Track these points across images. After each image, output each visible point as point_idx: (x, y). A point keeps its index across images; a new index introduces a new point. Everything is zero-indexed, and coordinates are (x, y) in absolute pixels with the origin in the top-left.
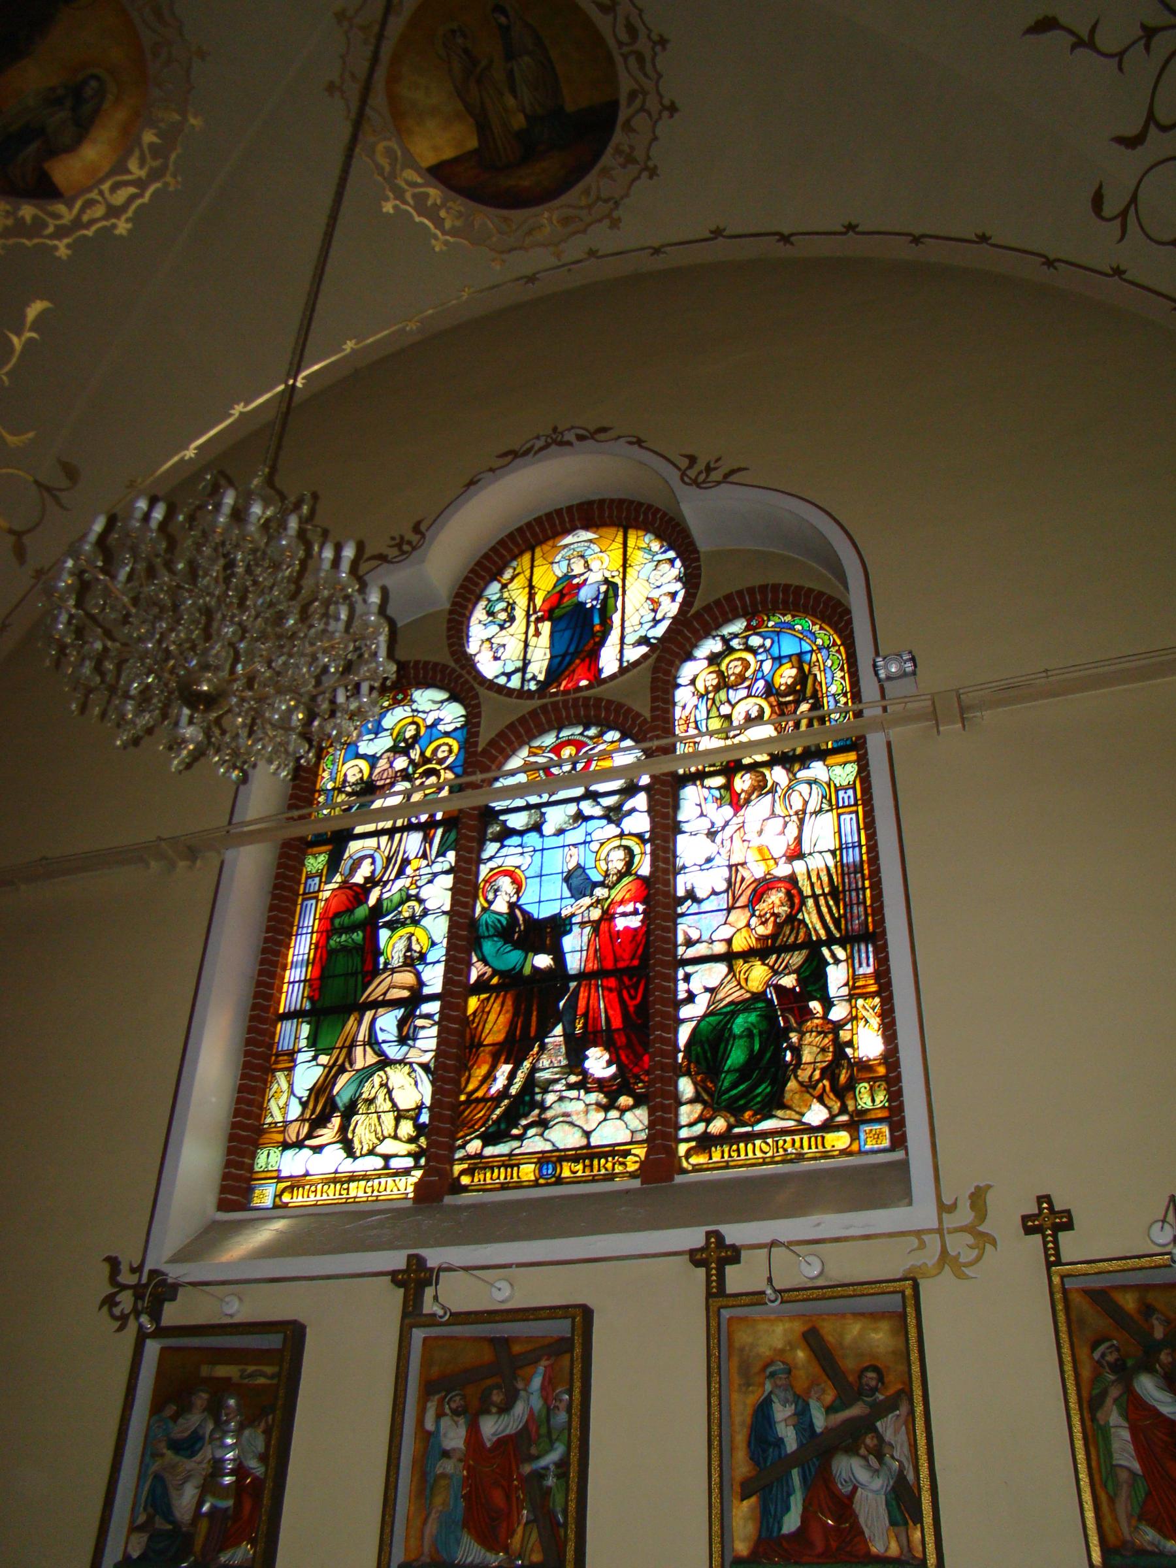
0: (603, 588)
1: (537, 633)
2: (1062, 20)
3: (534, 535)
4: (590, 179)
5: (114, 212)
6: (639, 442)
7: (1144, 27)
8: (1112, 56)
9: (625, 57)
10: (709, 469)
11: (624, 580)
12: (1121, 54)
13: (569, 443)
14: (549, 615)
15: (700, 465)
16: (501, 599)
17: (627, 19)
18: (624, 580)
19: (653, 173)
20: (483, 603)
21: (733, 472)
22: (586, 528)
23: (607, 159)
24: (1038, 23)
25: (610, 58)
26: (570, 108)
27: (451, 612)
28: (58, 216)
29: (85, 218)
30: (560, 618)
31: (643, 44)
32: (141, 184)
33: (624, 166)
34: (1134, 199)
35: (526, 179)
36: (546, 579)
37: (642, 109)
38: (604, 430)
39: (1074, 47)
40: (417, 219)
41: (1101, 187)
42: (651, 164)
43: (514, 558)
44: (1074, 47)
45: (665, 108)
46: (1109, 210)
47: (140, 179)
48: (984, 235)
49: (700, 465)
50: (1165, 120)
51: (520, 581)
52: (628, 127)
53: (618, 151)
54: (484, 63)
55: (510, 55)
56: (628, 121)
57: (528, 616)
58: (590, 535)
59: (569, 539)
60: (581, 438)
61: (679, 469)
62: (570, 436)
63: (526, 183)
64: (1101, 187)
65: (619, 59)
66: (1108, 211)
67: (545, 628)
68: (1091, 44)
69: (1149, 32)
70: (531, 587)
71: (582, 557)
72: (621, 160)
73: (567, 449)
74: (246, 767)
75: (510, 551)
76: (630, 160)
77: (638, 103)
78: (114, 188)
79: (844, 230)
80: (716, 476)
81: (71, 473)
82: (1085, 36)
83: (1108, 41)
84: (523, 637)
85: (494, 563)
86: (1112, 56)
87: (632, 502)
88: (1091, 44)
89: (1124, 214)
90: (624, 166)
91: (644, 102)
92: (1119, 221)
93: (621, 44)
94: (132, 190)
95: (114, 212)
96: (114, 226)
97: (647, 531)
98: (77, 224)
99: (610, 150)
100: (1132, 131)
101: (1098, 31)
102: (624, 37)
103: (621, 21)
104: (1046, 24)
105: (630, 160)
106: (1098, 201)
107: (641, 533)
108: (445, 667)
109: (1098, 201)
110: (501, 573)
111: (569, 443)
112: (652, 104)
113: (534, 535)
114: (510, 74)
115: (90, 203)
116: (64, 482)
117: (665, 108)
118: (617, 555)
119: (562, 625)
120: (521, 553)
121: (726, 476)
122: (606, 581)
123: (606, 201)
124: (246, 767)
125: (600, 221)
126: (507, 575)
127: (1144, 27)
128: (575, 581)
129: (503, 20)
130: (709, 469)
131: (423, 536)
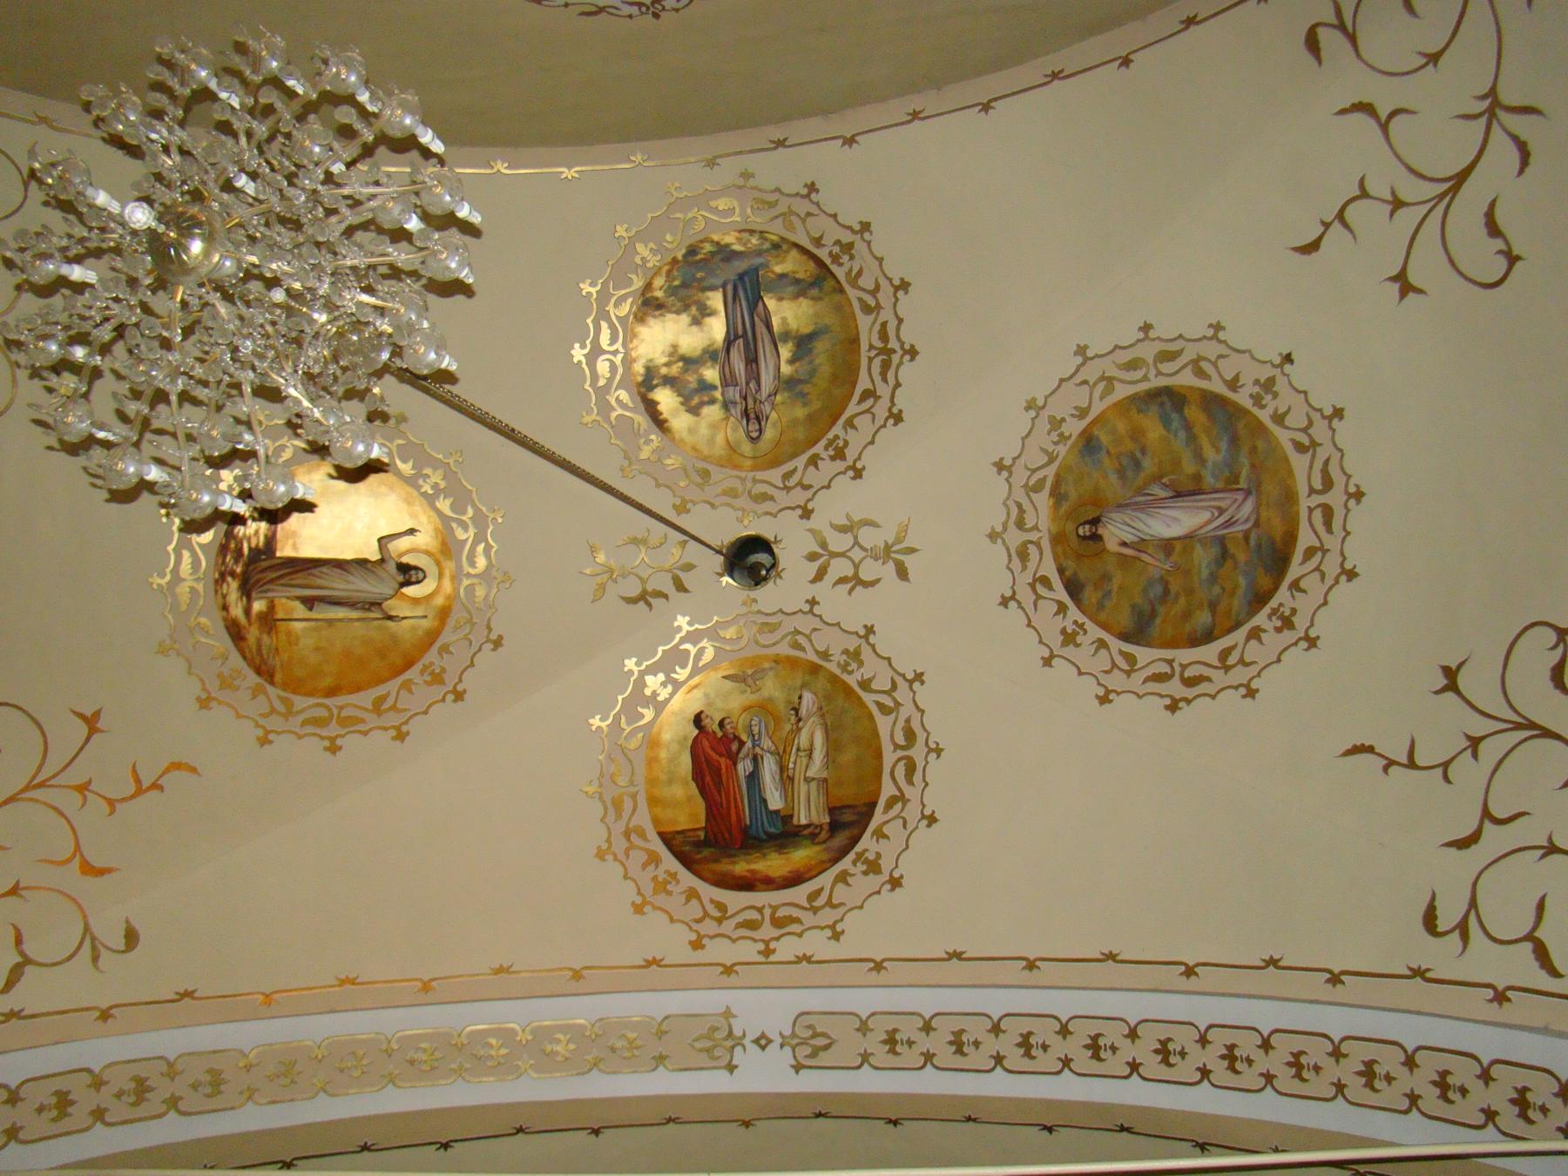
5: (596, 351)
12: (1446, 765)
29: (604, 325)
32: (602, 392)
34: (1473, 904)
39: (1386, 769)
40: (620, 698)
46: (1445, 921)
47: (608, 392)
48: (1500, 1004)
69: (1474, 743)
74: (281, 139)
77: (281, 708)
81: (1312, 44)
90: (852, 258)
91: (279, 713)
94: (602, 383)
95: (596, 351)
96: (583, 346)
98: (603, 315)
106: (1430, 920)
109: (1430, 920)
116: (1323, 34)
124: (281, 139)
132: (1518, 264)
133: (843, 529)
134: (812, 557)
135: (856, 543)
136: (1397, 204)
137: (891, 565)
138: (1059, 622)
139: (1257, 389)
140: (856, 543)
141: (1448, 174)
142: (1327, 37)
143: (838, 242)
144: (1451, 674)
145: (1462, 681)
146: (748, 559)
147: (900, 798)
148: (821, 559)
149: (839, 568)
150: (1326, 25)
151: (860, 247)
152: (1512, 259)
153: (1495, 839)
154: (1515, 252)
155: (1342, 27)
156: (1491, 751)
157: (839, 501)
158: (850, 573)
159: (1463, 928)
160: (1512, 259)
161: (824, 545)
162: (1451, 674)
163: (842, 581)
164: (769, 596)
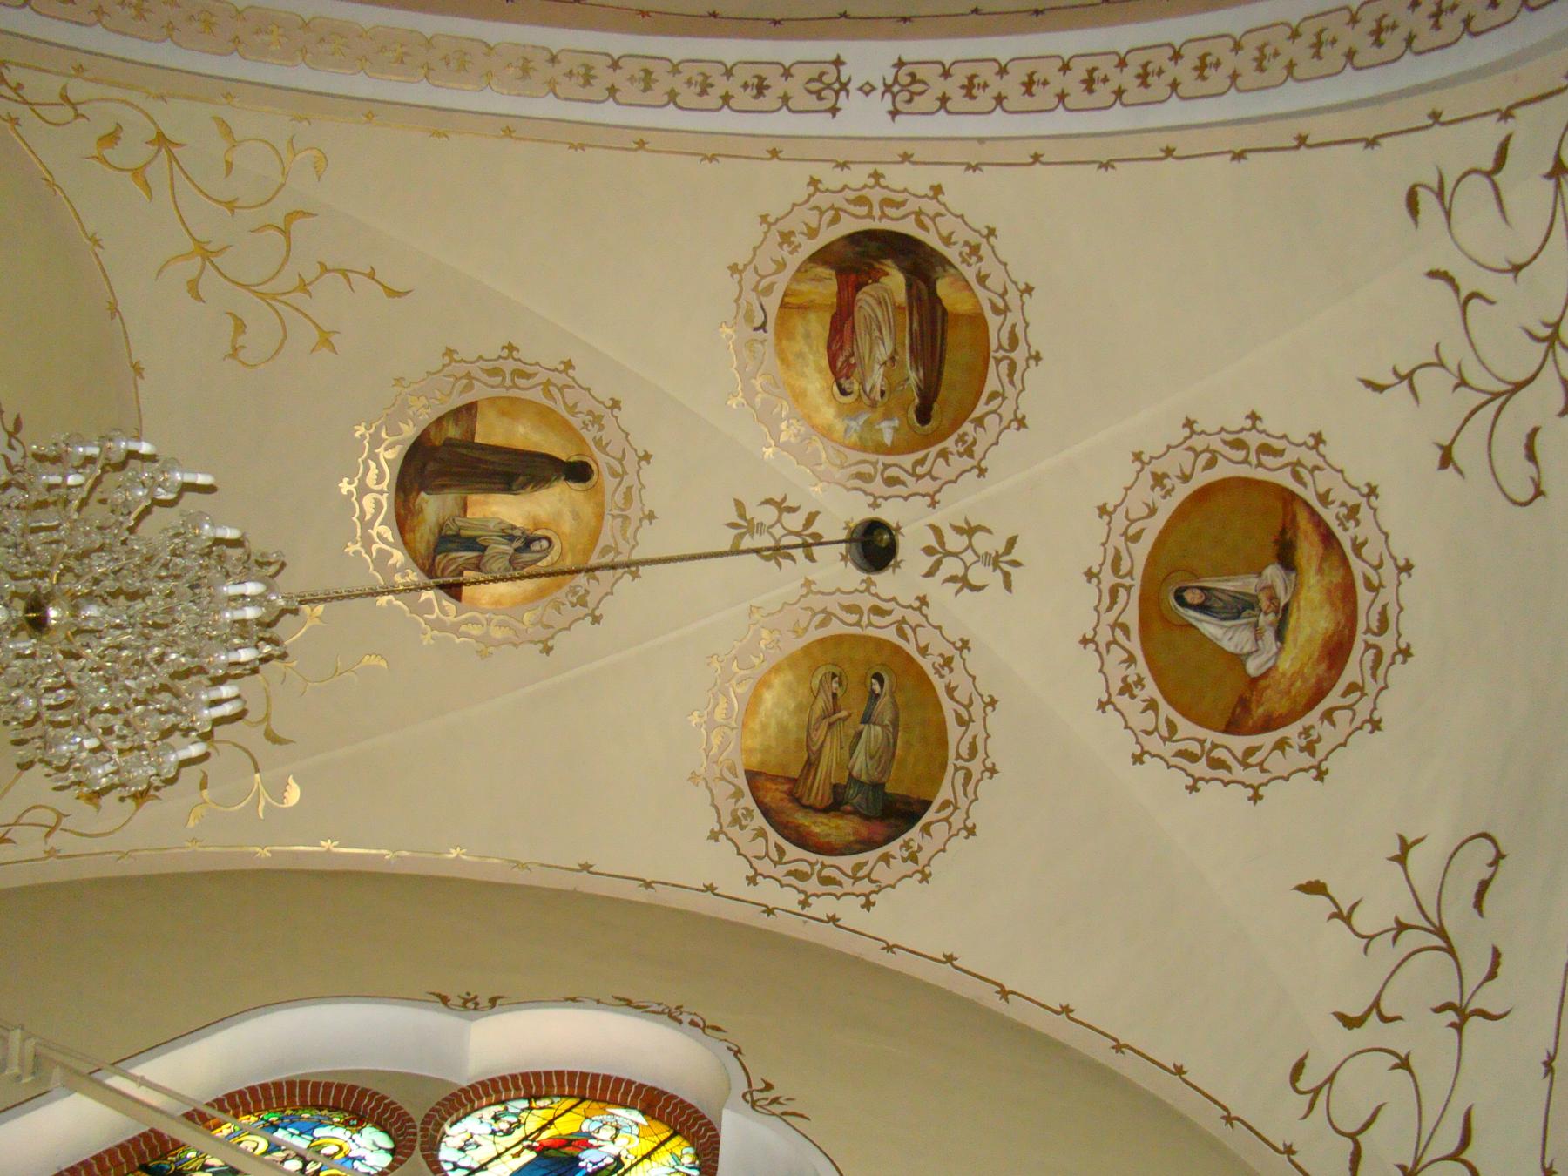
0: (609, 1160)
1: (518, 1155)
2: (1330, 890)
3: (593, 1088)
4: (872, 856)
6: (737, 1053)
7: (1397, 920)
8: (1363, 937)
9: (957, 769)
10: (775, 1100)
11: (632, 1166)
12: (1371, 938)
13: (680, 1022)
14: (542, 1151)
15: (771, 1095)
16: (517, 1115)
17: (975, 737)
18: (632, 1166)
19: (925, 878)
20: (499, 1108)
21: (794, 1114)
22: (644, 1112)
23: (894, 847)
24: (1309, 883)
25: (944, 766)
26: (889, 788)
27: (463, 1090)
28: (390, 447)
30: (547, 1157)
31: (976, 766)
33: (904, 860)
34: (1331, 1079)
35: (821, 826)
36: (566, 1126)
37: (946, 820)
38: (718, 1029)
41: (1305, 1057)
42: (927, 870)
43: (562, 1096)
44: (1333, 916)
45: (966, 828)
46: (1305, 1082)
49: (771, 1095)
50: (1388, 1013)
51: (549, 1114)
52: (926, 830)
53: (906, 845)
54: (844, 714)
55: (866, 719)
56: (929, 824)
57: (525, 1138)
58: (641, 1119)
59: (621, 1112)
60: (693, 1023)
61: (750, 1085)
62: (686, 1018)
63: (817, 829)
64: (1305, 1057)
65: (950, 769)
66: (1301, 1085)
67: (529, 1156)
68: (1347, 920)
69: (1401, 927)
70: (551, 1122)
71: (617, 1129)
72: (906, 854)
73: (676, 1024)
75: (561, 1085)
76: (913, 858)
78: (500, 625)
79: (1281, 1148)
80: (776, 1108)
82: (1345, 912)
83: (1361, 921)
84: (501, 1150)
85: (539, 1086)
86: (1363, 937)
87: (697, 1111)
88: (1347, 920)
89: (1316, 1091)
92: (1309, 1096)
93: (958, 757)
97: (692, 1145)
99: (900, 841)
100: (1354, 1011)
101: (1357, 910)
102: (964, 752)
103: (968, 739)
104: (1315, 888)
105: (913, 858)
106: (1298, 1069)
107: (685, 1143)
108: (422, 1150)
109: (1298, 1069)
110: (538, 1098)
111: (680, 1022)
112: (957, 820)
113: (593, 1088)
114: (859, 734)
115: (475, 621)
117: (966, 828)
118: (647, 1146)
119: (545, 1162)
120: (571, 1096)
121: (785, 1113)
122: (618, 1158)
123: (872, 881)
125: (1246, 786)
126: (541, 1103)
127: (1397, 920)
128: (591, 1141)
129: (877, 687)
130: (775, 1100)
131: (493, 1006)
132: (1540, 499)
133: (958, 530)
134: (929, 551)
135: (970, 546)
136: (1463, 383)
137: (999, 575)
138: (1122, 671)
139: (1136, 691)
140: (970, 546)
141: (1509, 379)
142: (1426, 200)
143: (966, 243)
144: (1405, 847)
145: (1413, 855)
146: (874, 547)
147: (1295, 466)
148: (937, 552)
149: (951, 567)
150: (1425, 186)
151: (726, 819)
152: (1539, 493)
153: (1372, 1031)
154: (1543, 487)
155: (1440, 194)
156: (1410, 940)
157: (962, 502)
158: (960, 572)
159: (1316, 1091)
160: (1539, 493)
161: (942, 543)
162: (1405, 847)
163: (952, 579)
164: (885, 582)
